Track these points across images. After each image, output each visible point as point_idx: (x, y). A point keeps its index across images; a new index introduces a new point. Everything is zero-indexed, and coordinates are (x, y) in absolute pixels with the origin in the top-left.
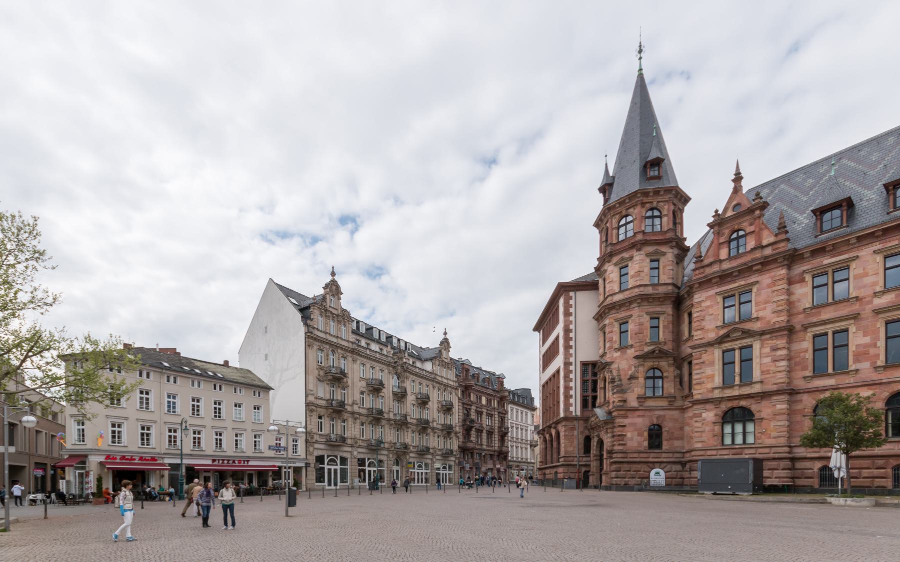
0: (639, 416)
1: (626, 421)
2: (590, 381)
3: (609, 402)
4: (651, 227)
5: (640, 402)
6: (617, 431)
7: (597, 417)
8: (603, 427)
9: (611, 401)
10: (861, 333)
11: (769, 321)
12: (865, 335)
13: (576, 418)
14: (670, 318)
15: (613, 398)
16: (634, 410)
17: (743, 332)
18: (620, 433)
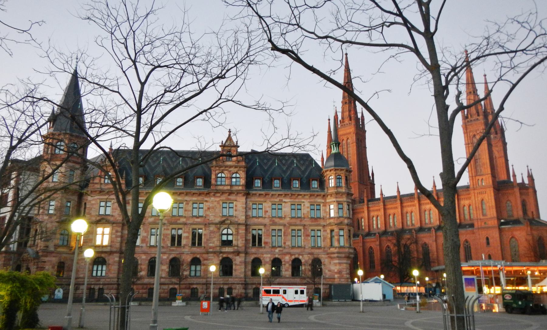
0: (54, 257)
1: (46, 259)
2: (25, 229)
3: (37, 245)
4: (268, 24)
5: (55, 248)
6: (40, 265)
7: (29, 254)
8: (32, 261)
9: (39, 245)
10: (144, 232)
11: (116, 218)
12: (145, 232)
13: (13, 252)
14: (76, 203)
15: (41, 244)
16: (52, 252)
17: (106, 221)
18: (42, 266)
